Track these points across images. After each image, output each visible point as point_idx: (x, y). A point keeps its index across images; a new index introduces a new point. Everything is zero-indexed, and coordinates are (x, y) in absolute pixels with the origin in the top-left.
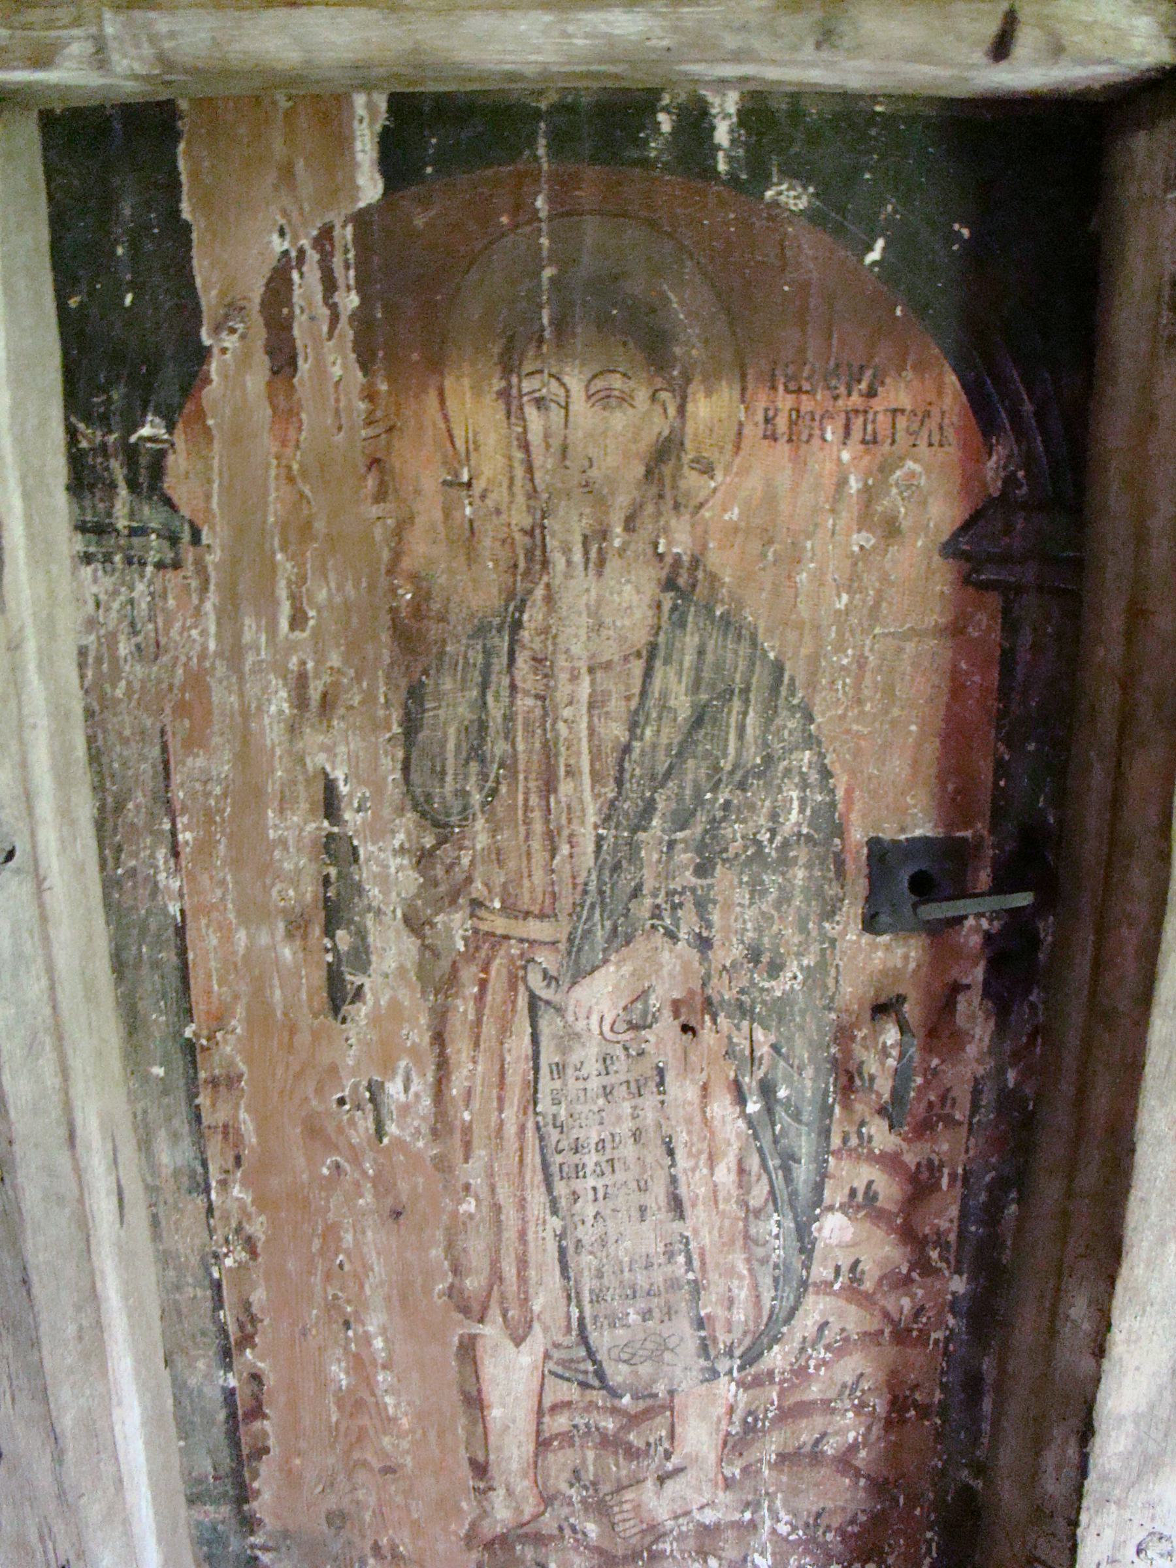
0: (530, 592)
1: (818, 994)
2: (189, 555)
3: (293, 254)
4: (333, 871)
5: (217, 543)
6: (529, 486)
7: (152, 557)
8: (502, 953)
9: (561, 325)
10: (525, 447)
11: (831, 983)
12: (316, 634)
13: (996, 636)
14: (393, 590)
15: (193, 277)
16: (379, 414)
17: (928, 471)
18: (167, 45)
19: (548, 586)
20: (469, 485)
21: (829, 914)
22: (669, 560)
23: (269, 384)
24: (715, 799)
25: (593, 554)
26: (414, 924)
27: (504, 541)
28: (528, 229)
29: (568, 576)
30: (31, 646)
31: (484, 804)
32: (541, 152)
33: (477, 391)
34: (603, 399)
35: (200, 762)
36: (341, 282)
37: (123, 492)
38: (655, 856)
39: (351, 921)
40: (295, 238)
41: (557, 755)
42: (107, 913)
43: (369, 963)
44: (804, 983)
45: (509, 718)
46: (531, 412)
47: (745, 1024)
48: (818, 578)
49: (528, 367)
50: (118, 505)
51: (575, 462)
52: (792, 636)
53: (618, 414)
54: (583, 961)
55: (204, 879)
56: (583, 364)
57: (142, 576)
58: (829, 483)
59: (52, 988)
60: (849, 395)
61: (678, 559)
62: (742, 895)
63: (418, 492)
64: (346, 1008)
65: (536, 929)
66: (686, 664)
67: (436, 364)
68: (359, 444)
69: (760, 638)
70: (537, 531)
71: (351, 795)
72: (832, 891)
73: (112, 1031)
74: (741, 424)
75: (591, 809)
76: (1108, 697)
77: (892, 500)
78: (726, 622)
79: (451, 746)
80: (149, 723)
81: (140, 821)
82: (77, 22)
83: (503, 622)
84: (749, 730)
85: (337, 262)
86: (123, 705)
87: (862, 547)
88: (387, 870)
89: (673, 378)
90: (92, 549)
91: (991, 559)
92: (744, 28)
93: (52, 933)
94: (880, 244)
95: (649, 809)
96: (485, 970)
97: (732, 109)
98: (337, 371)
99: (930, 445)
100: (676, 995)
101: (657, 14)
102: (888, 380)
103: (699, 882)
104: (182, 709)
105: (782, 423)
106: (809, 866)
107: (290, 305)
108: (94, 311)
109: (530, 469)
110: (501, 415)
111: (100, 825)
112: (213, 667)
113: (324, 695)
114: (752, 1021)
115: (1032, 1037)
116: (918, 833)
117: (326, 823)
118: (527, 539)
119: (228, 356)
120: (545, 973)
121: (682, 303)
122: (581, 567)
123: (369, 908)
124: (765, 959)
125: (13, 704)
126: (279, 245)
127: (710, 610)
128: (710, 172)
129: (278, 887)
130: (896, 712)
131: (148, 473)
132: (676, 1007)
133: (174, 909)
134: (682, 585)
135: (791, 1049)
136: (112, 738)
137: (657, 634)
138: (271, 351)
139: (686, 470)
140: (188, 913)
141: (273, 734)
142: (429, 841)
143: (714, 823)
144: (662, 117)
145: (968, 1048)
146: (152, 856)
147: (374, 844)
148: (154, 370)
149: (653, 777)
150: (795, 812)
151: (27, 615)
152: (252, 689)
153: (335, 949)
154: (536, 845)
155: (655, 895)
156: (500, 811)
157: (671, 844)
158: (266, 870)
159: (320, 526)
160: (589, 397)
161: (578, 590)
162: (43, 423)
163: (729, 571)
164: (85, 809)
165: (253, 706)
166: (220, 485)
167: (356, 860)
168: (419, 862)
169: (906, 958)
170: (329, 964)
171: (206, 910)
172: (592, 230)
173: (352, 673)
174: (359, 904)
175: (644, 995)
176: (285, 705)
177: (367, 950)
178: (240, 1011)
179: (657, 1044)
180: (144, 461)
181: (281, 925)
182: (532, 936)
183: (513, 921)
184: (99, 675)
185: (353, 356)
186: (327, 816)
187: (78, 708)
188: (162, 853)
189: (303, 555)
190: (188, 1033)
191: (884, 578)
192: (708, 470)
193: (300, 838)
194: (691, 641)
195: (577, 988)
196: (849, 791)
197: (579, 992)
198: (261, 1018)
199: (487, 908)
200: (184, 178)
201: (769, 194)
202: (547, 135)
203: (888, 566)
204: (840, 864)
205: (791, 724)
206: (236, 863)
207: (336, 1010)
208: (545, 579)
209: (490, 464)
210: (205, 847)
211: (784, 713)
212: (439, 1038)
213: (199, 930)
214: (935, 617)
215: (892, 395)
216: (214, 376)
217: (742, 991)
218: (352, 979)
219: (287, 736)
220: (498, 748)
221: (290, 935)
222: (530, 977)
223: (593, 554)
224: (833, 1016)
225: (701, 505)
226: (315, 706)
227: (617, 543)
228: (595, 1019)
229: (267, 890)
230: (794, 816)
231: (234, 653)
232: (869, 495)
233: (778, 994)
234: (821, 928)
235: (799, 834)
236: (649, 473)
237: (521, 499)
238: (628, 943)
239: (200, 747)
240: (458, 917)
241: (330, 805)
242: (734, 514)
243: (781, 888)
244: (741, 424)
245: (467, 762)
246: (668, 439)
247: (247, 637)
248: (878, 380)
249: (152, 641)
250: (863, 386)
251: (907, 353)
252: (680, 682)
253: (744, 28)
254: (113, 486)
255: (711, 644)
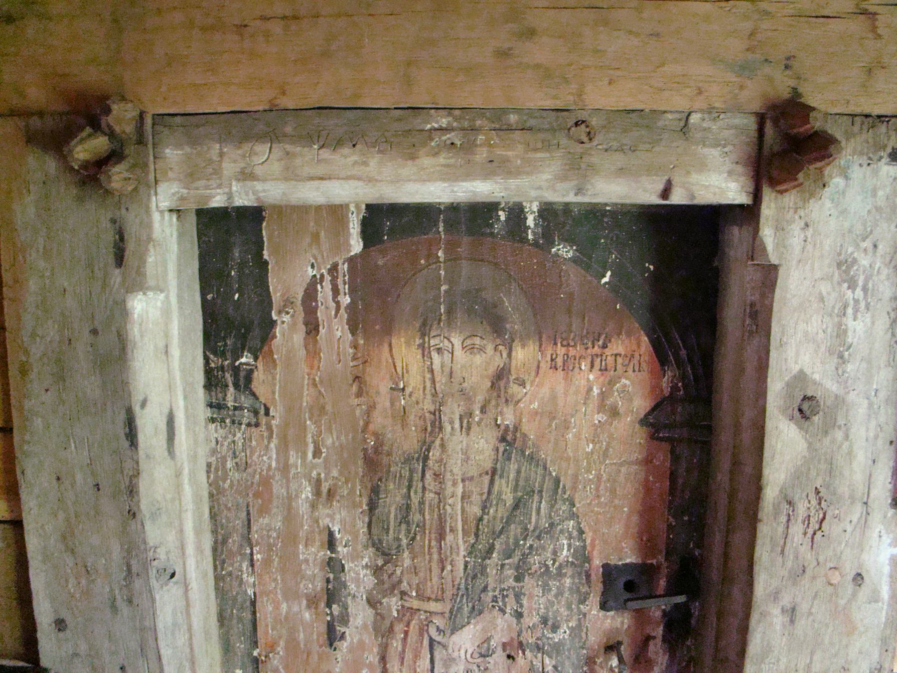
0: (433, 442)
1: (577, 640)
2: (263, 420)
3: (318, 277)
4: (331, 576)
5: (277, 415)
6: (433, 391)
7: (245, 421)
8: (416, 617)
9: (450, 312)
10: (432, 371)
11: (584, 636)
12: (326, 460)
13: (668, 464)
14: (365, 440)
15: (268, 287)
16: (359, 355)
17: (632, 383)
18: (261, 195)
19: (442, 439)
20: (403, 389)
21: (583, 601)
22: (502, 427)
23: (305, 339)
24: (525, 544)
25: (465, 424)
26: (372, 602)
27: (420, 417)
28: (434, 266)
29: (452, 434)
30: (186, 471)
31: (408, 545)
32: (441, 229)
33: (408, 344)
34: (471, 349)
35: (266, 521)
36: (342, 291)
37: (231, 389)
38: (494, 572)
39: (341, 601)
40: (319, 269)
41: (445, 521)
42: (216, 593)
43: (349, 621)
44: (570, 635)
45: (422, 503)
46: (435, 355)
47: (540, 655)
48: (578, 436)
49: (432, 334)
50: (229, 395)
51: (457, 379)
52: (564, 465)
53: (478, 356)
54: (457, 622)
55: (266, 578)
56: (461, 333)
57: (240, 429)
58: (583, 391)
59: (191, 638)
60: (593, 347)
61: (507, 426)
62: (538, 591)
63: (378, 393)
64: (336, 644)
65: (433, 606)
66: (511, 479)
67: (388, 330)
68: (349, 369)
69: (548, 466)
70: (437, 413)
71: (342, 538)
72: (584, 589)
73: (216, 651)
74: (539, 362)
75: (462, 548)
76: (722, 499)
77: (616, 398)
78: (531, 458)
79: (392, 516)
80: (241, 501)
81: (235, 549)
82: (219, 186)
83: (420, 455)
84: (542, 510)
85: (340, 281)
86: (228, 492)
87: (599, 421)
88: (359, 576)
89: (505, 339)
90: (215, 416)
91: (666, 426)
92: (540, 188)
93: (192, 611)
94: (609, 273)
95: (491, 549)
96: (408, 625)
97: (535, 209)
98: (339, 334)
99: (634, 371)
100: (504, 640)
101: (496, 183)
102: (613, 340)
103: (517, 584)
104: (257, 495)
105: (559, 361)
106: (573, 577)
107: (316, 301)
108: (219, 301)
109: (433, 382)
110: (419, 356)
111: (215, 550)
112: (274, 475)
113: (329, 490)
114: (543, 653)
115: (689, 662)
116: (628, 561)
117: (329, 552)
118: (432, 416)
119: (285, 324)
120: (438, 629)
121: (510, 303)
122: (459, 430)
123: (349, 594)
124: (550, 623)
125: (177, 502)
126: (311, 272)
127: (523, 452)
128: (524, 240)
129: (304, 582)
130: (617, 502)
131: (244, 382)
132: (504, 646)
133: (250, 592)
134: (509, 440)
135: (563, 668)
136: (222, 507)
137: (496, 464)
138: (306, 324)
139: (511, 384)
140: (258, 594)
141: (303, 508)
142: (380, 562)
143: (525, 556)
144: (501, 213)
145: (655, 668)
146: (241, 566)
147: (353, 563)
148: (248, 330)
149: (494, 533)
150: (565, 551)
151: (185, 456)
152: (293, 486)
153: (331, 614)
154: (435, 566)
155: (494, 591)
156: (417, 549)
157: (503, 566)
158: (298, 574)
159: (329, 408)
160: (463, 348)
161: (456, 441)
162: (194, 358)
163: (533, 432)
164: (208, 542)
165: (294, 494)
166: (280, 387)
167: (343, 570)
168: (375, 573)
169: (622, 623)
170: (328, 622)
171: (267, 594)
172: (465, 267)
173: (343, 479)
174: (344, 592)
175: (488, 640)
176: (310, 495)
177: (348, 615)
178: (282, 643)
179: (495, 665)
180: (242, 374)
181: (305, 602)
182: (432, 610)
183: (422, 602)
184: (216, 477)
185: (347, 327)
186: (329, 549)
187: (205, 494)
188: (245, 565)
189: (321, 421)
190: (255, 653)
191: (611, 436)
192: (523, 384)
193: (315, 560)
194: (513, 467)
195: (454, 636)
196: (593, 540)
197: (455, 638)
198: (292, 645)
199: (409, 596)
200: (265, 239)
201: (553, 250)
202: (444, 221)
203: (612, 430)
204: (588, 576)
205: (564, 508)
206: (283, 570)
207: (331, 645)
208: (441, 435)
209: (414, 379)
210: (267, 562)
211: (560, 502)
212: (383, 659)
213: (262, 602)
214: (636, 456)
215: (615, 347)
216: (278, 334)
217: (538, 639)
218: (340, 629)
219: (310, 510)
220: (416, 517)
221: (309, 607)
222: (430, 629)
223: (465, 424)
224: (585, 651)
225: (519, 401)
226: (325, 495)
227: (477, 419)
228: (462, 652)
229: (298, 584)
230: (565, 552)
231: (285, 468)
232: (603, 395)
233: (557, 640)
234: (579, 608)
235: (568, 561)
236: (493, 384)
237: (429, 397)
238: (480, 614)
239: (266, 513)
240: (394, 599)
241: (331, 543)
242: (536, 405)
243: (558, 588)
244: (539, 362)
245: (400, 525)
246: (503, 369)
247: (292, 461)
248: (608, 339)
249: (244, 461)
250: (601, 343)
251: (622, 327)
252: (507, 487)
253: (540, 188)
254: (227, 386)
255: (523, 469)
